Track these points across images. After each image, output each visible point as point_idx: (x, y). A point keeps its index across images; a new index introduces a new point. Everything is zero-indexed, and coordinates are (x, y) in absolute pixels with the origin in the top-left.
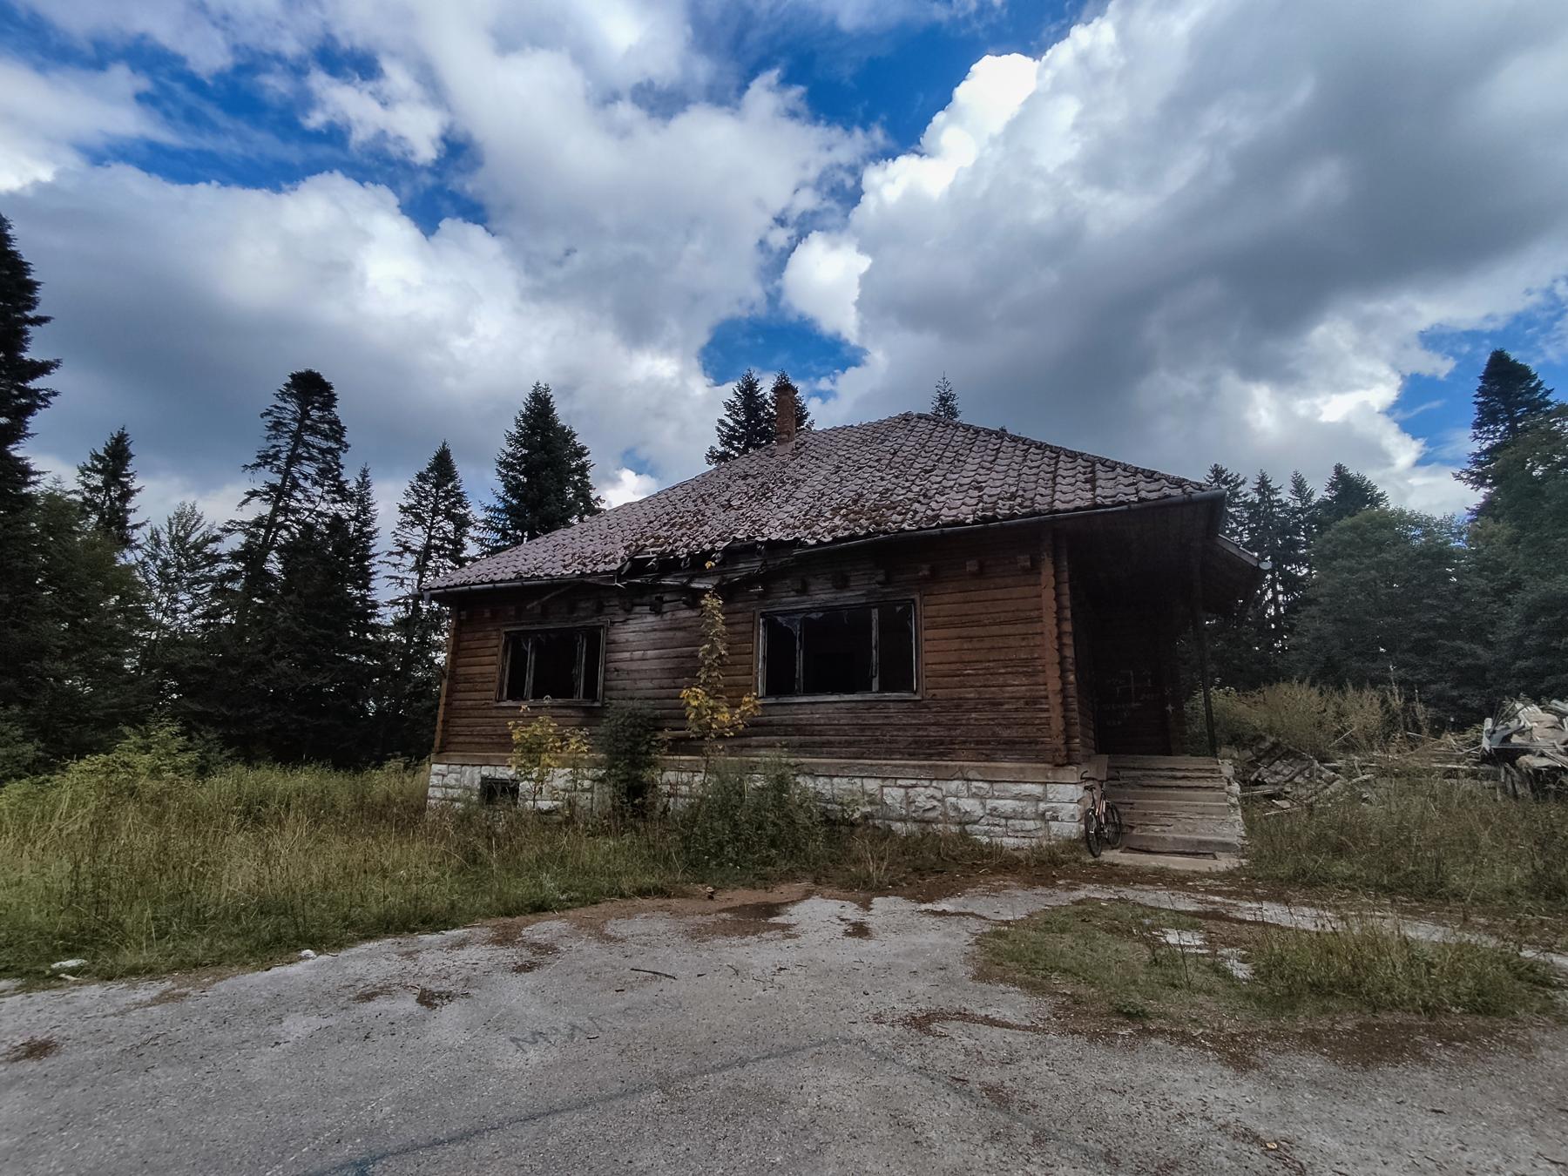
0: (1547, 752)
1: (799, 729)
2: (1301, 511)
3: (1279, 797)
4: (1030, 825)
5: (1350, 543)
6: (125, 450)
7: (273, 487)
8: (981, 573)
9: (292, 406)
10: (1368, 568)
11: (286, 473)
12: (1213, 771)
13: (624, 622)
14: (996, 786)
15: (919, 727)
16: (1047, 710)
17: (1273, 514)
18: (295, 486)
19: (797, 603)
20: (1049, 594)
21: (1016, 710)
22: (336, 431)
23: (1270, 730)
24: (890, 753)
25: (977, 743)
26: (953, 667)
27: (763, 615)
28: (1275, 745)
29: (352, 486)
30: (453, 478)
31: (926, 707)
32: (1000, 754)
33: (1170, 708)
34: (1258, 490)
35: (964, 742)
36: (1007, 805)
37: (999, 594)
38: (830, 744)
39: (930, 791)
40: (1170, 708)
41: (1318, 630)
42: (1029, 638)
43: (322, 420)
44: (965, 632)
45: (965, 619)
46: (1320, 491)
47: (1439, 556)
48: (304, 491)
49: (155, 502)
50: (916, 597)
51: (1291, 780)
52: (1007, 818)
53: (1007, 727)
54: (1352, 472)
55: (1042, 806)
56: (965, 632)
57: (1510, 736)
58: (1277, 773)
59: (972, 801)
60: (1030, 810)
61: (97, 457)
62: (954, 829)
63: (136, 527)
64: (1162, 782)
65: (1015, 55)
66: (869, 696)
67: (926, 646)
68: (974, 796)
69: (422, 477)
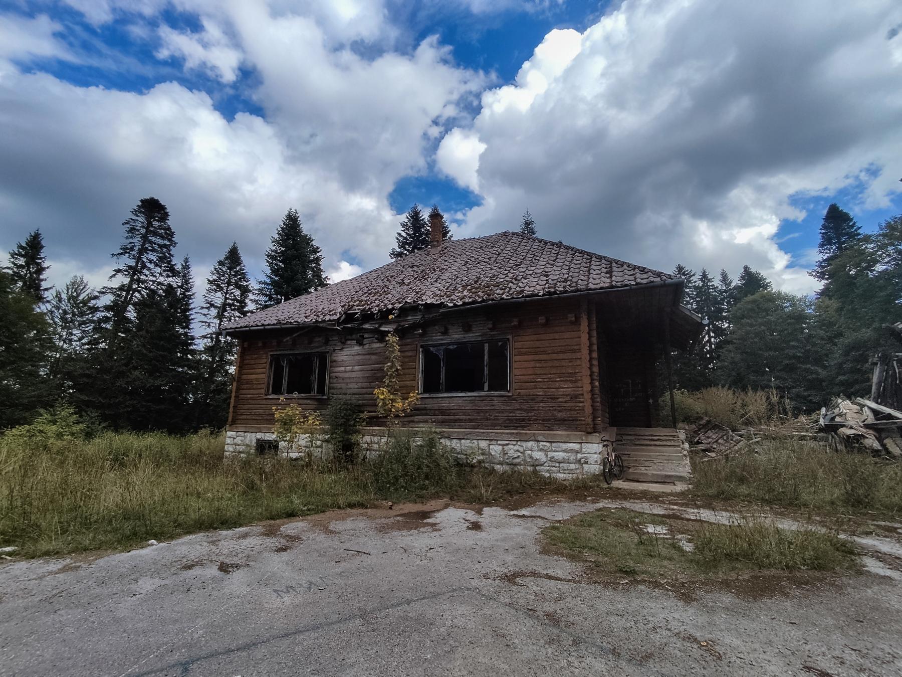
1: (442, 412)
2: (725, 291)
3: (710, 451)
4: (572, 466)
6: (39, 243)
7: (130, 267)
8: (547, 324)
9: (142, 219)
11: (138, 259)
12: (674, 436)
13: (341, 350)
14: (554, 445)
15: (513, 411)
16: (583, 402)
18: (144, 266)
19: (442, 340)
20: (585, 337)
21: (566, 402)
22: (169, 234)
23: (706, 414)
24: (494, 426)
25: (543, 420)
26: (531, 377)
27: (422, 346)
28: (709, 422)
29: (178, 267)
30: (240, 264)
31: (514, 400)
32: (556, 427)
33: (651, 401)
34: (701, 280)
35: (536, 420)
36: (560, 455)
37: (557, 336)
38: (460, 420)
39: (517, 447)
40: (651, 401)
42: (572, 362)
43: (160, 227)
44: (537, 357)
45: (538, 350)
46: (736, 281)
47: (799, 317)
48: (149, 269)
49: (57, 274)
50: (510, 337)
51: (717, 441)
52: (559, 463)
53: (560, 411)
55: (579, 456)
56: (537, 357)
57: (835, 417)
58: (709, 438)
59: (540, 453)
60: (572, 458)
61: (21, 247)
62: (530, 469)
63: (46, 289)
64: (648, 443)
66: (482, 394)
67: (515, 365)
68: (541, 450)
69: (221, 263)
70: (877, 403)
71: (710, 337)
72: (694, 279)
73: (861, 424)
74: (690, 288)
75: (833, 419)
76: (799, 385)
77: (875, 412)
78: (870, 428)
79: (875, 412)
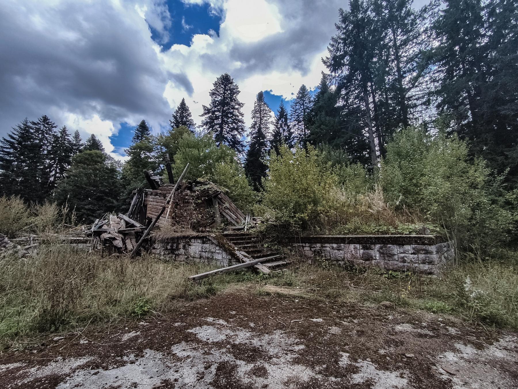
0: (112, 232)
2: (75, 145)
5: (87, 159)
10: (90, 169)
17: (64, 143)
34: (61, 133)
41: (65, 187)
46: (84, 141)
47: (113, 171)
54: (97, 139)
57: (103, 225)
65: (182, 45)
70: (130, 218)
71: (56, 173)
72: (54, 129)
73: (116, 230)
74: (50, 135)
75: (100, 227)
76: (101, 209)
77: (127, 223)
78: (120, 233)
79: (127, 223)
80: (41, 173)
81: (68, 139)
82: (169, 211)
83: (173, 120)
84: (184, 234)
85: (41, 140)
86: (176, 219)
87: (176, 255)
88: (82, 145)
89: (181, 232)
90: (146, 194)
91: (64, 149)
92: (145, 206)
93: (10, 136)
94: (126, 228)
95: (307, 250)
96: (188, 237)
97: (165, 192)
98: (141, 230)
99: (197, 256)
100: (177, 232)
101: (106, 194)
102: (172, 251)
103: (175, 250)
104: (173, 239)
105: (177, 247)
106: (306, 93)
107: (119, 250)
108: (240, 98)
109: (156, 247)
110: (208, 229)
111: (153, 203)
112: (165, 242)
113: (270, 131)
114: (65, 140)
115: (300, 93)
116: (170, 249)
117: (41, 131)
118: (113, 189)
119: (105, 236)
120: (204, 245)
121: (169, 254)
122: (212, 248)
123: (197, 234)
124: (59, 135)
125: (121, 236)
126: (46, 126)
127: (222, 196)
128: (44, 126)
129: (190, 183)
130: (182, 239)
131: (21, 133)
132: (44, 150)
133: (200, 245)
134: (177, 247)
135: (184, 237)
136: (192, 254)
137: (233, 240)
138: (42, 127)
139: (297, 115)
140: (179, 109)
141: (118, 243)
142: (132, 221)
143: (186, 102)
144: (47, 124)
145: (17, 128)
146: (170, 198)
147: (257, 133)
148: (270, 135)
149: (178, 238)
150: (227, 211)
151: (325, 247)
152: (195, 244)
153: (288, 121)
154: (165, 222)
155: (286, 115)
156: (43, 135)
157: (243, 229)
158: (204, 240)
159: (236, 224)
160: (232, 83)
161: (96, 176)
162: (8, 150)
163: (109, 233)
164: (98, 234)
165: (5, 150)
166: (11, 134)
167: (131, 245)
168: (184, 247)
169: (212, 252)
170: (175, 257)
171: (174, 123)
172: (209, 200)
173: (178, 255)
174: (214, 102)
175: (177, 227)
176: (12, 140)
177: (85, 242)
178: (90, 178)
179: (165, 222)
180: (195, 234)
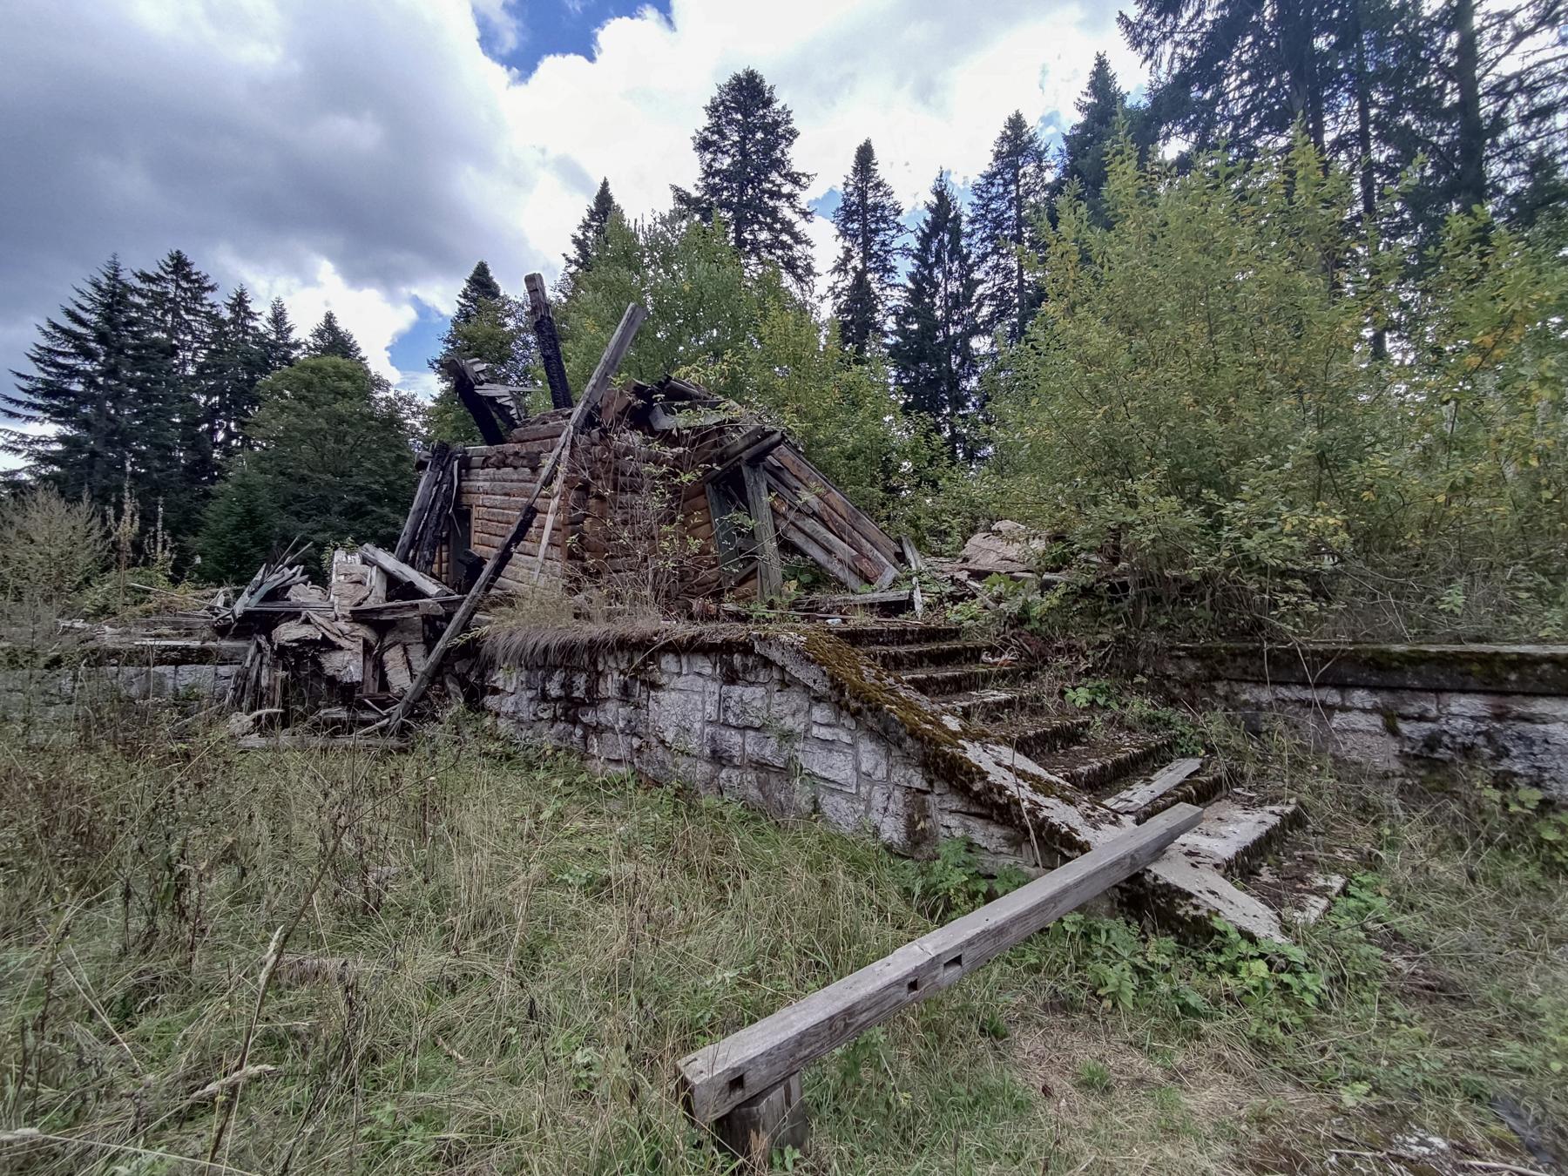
17: (244, 341)
34: (232, 308)
47: (391, 422)
72: (210, 297)
74: (196, 313)
78: (363, 622)
80: (188, 439)
81: (254, 328)
82: (550, 520)
83: (573, 252)
84: (621, 628)
85: (172, 332)
86: (586, 559)
87: (586, 726)
88: (297, 345)
89: (609, 617)
90: (466, 464)
91: (250, 360)
92: (464, 516)
93: (70, 314)
94: (388, 599)
95: (1358, 726)
96: (642, 645)
97: (535, 447)
98: (442, 611)
99: (693, 745)
100: (588, 617)
101: (376, 498)
102: (571, 709)
103: (582, 703)
104: (568, 651)
105: (591, 690)
106: (1025, 138)
107: (346, 693)
108: (798, 156)
109: (500, 685)
110: (731, 607)
111: (492, 496)
112: (540, 662)
113: (897, 281)
114: (246, 333)
115: (1004, 138)
116: (558, 699)
117: (170, 300)
118: (393, 482)
119: (288, 632)
120: (736, 691)
121: (554, 719)
122: (788, 710)
123: (694, 630)
124: (227, 314)
125: (363, 632)
126: (185, 285)
127: (782, 456)
128: (178, 286)
129: (639, 391)
130: (611, 651)
131: (102, 304)
132: (184, 363)
133: (713, 687)
134: (591, 690)
135: (623, 645)
136: (669, 737)
137: (917, 661)
138: (171, 288)
139: (993, 220)
140: (592, 214)
141: (347, 664)
142: (410, 574)
143: (612, 190)
144: (187, 277)
145: (90, 290)
146: (557, 462)
147: (851, 288)
148: (896, 293)
149: (594, 647)
150: (810, 524)
151: (1529, 719)
152: (679, 683)
153: (963, 243)
154: (536, 573)
155: (957, 217)
156: (176, 315)
157: (907, 605)
158: (735, 660)
159: (853, 581)
160: (768, 103)
161: (340, 439)
162: (71, 362)
163: (307, 621)
164: (257, 624)
165: (60, 360)
166: (72, 307)
167: (403, 672)
168: (625, 692)
169: (787, 736)
170: (585, 738)
171: (576, 262)
172: (730, 474)
173: (598, 729)
174: (710, 172)
175: (592, 596)
176: (83, 330)
177: (203, 656)
178: (323, 447)
179: (536, 573)
180: (682, 630)
